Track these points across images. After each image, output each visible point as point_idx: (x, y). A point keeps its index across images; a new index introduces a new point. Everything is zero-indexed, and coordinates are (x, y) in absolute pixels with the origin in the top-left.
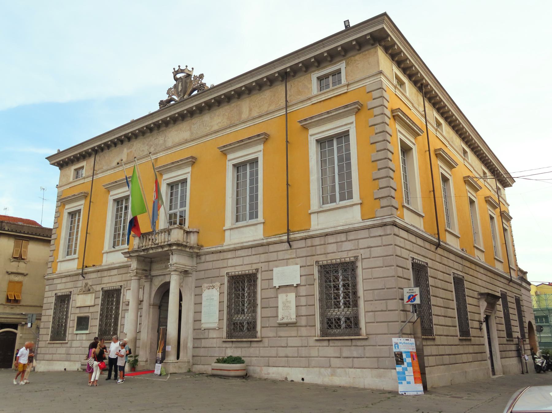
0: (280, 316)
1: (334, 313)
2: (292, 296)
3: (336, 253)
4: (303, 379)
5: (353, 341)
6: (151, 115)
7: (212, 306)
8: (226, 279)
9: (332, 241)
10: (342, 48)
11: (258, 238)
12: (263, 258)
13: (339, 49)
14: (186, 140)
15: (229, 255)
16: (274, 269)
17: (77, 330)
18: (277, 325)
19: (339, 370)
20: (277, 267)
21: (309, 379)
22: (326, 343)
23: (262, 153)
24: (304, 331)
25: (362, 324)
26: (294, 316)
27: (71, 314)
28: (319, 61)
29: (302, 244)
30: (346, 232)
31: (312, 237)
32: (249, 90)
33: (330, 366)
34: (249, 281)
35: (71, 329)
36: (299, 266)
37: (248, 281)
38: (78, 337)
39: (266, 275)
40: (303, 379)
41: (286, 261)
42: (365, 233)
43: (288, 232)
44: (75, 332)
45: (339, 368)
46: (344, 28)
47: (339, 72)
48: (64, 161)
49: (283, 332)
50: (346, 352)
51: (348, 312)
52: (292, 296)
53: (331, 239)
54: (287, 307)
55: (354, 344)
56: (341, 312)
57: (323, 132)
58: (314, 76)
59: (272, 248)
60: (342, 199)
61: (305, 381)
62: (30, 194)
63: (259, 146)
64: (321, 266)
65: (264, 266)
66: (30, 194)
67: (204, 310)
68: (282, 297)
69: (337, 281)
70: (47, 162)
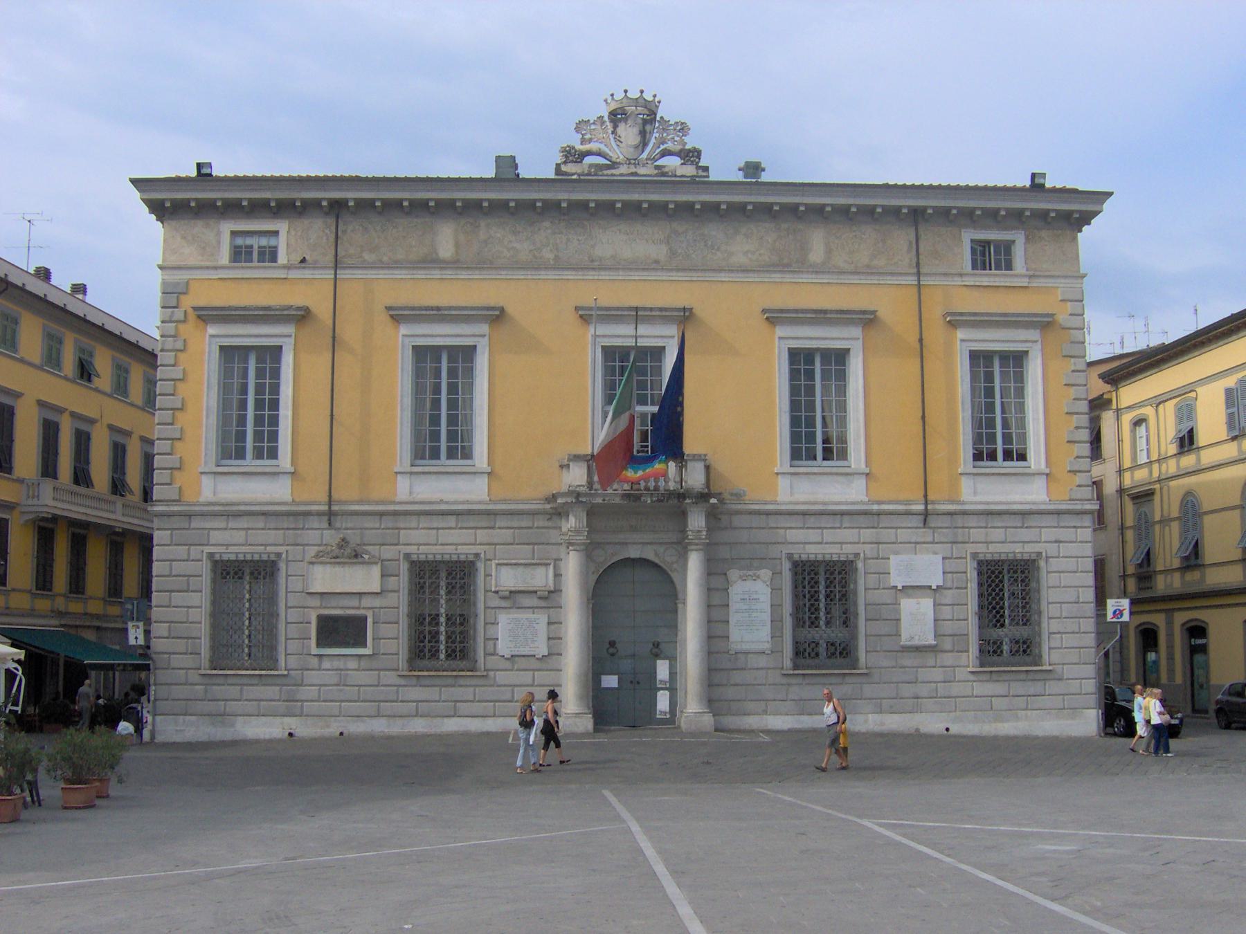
0: (903, 638)
2: (925, 606)
3: (1005, 543)
4: (947, 729)
6: (178, 180)
7: (759, 611)
8: (787, 566)
10: (569, 205)
11: (473, 497)
12: (482, 535)
13: (219, 204)
14: (657, 262)
17: (364, 645)
18: (897, 648)
20: (897, 553)
21: (955, 729)
23: (292, 340)
27: (287, 607)
28: (992, 217)
29: (945, 522)
30: (804, 514)
31: (964, 513)
32: (844, 214)
34: (255, 575)
35: (293, 646)
36: (939, 557)
38: (326, 664)
40: (947, 729)
42: (1051, 520)
43: (330, 503)
44: (315, 651)
46: (551, 175)
47: (276, 233)
48: (179, 202)
49: (908, 660)
50: (1017, 688)
52: (925, 606)
54: (917, 620)
56: (823, 634)
58: (968, 236)
59: (885, 521)
60: (259, 454)
61: (951, 732)
64: (216, 561)
65: (869, 550)
67: (733, 619)
69: (1005, 592)
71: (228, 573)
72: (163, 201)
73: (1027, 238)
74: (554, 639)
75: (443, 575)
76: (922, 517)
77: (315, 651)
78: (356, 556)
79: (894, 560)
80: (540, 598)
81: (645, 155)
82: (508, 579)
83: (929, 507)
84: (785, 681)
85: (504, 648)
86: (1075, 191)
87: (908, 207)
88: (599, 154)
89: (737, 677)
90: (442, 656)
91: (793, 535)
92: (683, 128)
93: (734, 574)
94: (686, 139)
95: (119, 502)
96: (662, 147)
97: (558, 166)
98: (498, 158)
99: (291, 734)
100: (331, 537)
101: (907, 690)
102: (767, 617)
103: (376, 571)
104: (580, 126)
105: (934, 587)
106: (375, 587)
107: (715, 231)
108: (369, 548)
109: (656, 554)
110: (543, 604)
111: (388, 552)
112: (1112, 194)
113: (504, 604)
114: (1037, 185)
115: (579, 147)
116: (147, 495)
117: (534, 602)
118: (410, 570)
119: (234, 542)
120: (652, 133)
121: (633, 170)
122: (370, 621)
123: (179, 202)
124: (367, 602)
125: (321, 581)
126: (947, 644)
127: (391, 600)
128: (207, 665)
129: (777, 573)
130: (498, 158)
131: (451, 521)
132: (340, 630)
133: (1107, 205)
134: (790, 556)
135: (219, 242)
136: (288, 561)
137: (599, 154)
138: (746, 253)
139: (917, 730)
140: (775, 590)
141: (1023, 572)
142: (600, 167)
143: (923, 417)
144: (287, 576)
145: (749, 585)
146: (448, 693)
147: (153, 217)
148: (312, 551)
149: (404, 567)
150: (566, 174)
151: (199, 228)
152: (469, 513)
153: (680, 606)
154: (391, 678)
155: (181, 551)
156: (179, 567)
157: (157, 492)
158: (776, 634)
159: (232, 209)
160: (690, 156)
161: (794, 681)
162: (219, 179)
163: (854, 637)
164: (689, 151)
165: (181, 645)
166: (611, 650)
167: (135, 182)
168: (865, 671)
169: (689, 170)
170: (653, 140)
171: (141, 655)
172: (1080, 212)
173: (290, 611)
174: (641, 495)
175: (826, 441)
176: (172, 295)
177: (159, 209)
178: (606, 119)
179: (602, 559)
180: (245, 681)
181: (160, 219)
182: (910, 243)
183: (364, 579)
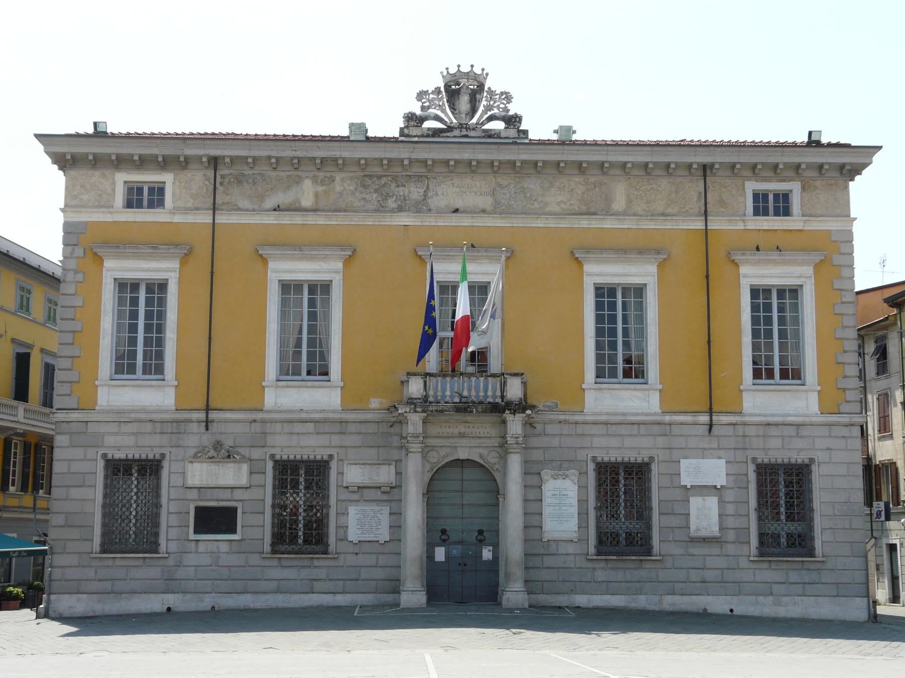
0: (693, 527)
1: (773, 527)
2: (712, 502)
3: (779, 451)
4: (732, 611)
5: (147, 560)
8: (591, 467)
9: (776, 434)
15: (595, 430)
16: (682, 460)
18: (687, 539)
19: (785, 599)
20: (685, 458)
22: (766, 565)
24: (731, 549)
25: (818, 544)
26: (716, 529)
31: (745, 424)
33: (771, 594)
34: (142, 472)
36: (723, 461)
37: (139, 471)
39: (176, 467)
40: (732, 611)
41: (703, 453)
43: (208, 409)
45: (784, 596)
49: (696, 550)
50: (794, 576)
51: (795, 527)
52: (712, 502)
53: (773, 431)
54: (704, 515)
55: (805, 567)
56: (623, 525)
57: (131, 270)
62: (34, 217)
63: (806, 268)
66: (34, 217)
67: (547, 511)
68: (695, 503)
70: (40, 147)
71: (119, 471)
72: (64, 154)
73: (803, 189)
74: (397, 527)
75: (302, 472)
76: (707, 427)
77: (192, 536)
78: (229, 457)
79: (684, 463)
80: (384, 493)
81: (474, 120)
82: (354, 475)
83: (714, 418)
84: (590, 565)
85: (354, 534)
86: (848, 146)
87: (698, 164)
88: (437, 118)
89: (549, 561)
90: (300, 541)
91: (597, 442)
92: (507, 97)
93: (546, 474)
94: (509, 106)
95: (21, 406)
96: (489, 113)
97: (402, 129)
98: (463, 89)
99: (169, 609)
100: (207, 439)
101: (694, 575)
102: (574, 510)
103: (245, 467)
104: (421, 95)
105: (719, 487)
106: (244, 481)
107: (533, 184)
108: (239, 450)
109: (481, 456)
110: (385, 497)
111: (256, 454)
112: (880, 148)
113: (355, 497)
114: (813, 143)
115: (418, 112)
116: (47, 401)
117: (378, 495)
118: (274, 468)
119: (124, 446)
120: (480, 101)
121: (464, 132)
122: (239, 511)
123: (79, 155)
124: (238, 494)
125: (197, 477)
126: (731, 536)
127: (256, 494)
128: (98, 550)
129: (583, 474)
130: (463, 89)
131: (310, 427)
132: (215, 519)
133: (877, 158)
134: (594, 459)
135: (114, 190)
136: (170, 461)
137: (437, 118)
138: (558, 204)
139: (705, 610)
140: (582, 487)
141: (797, 475)
142: (436, 132)
143: (709, 342)
144: (170, 473)
145: (560, 483)
146: (304, 573)
147: (56, 167)
148: (192, 452)
149: (270, 465)
150: (408, 136)
151: (95, 177)
152: (325, 421)
153: (501, 500)
154: (255, 559)
155: (79, 453)
156: (76, 467)
157: (57, 402)
158: (583, 524)
159: (121, 162)
160: (513, 121)
161: (597, 565)
162: (113, 136)
163: (649, 527)
164: (512, 117)
165: (75, 534)
166: (443, 537)
167: (38, 136)
168: (659, 558)
169: (512, 133)
170: (481, 108)
171: (36, 542)
172: (851, 164)
173: (171, 503)
174: (469, 407)
175: (628, 361)
176: (73, 234)
177: (64, 162)
178: (442, 89)
179: (435, 460)
180: (132, 563)
181: (61, 168)
182: (700, 193)
183: (231, 475)
